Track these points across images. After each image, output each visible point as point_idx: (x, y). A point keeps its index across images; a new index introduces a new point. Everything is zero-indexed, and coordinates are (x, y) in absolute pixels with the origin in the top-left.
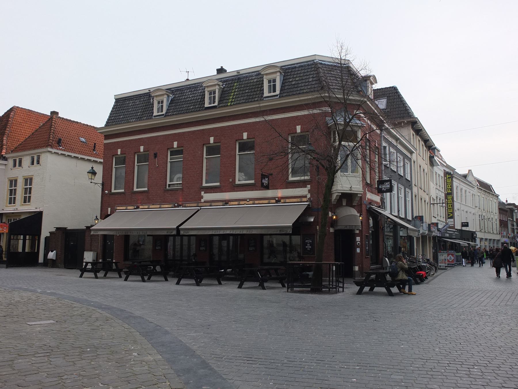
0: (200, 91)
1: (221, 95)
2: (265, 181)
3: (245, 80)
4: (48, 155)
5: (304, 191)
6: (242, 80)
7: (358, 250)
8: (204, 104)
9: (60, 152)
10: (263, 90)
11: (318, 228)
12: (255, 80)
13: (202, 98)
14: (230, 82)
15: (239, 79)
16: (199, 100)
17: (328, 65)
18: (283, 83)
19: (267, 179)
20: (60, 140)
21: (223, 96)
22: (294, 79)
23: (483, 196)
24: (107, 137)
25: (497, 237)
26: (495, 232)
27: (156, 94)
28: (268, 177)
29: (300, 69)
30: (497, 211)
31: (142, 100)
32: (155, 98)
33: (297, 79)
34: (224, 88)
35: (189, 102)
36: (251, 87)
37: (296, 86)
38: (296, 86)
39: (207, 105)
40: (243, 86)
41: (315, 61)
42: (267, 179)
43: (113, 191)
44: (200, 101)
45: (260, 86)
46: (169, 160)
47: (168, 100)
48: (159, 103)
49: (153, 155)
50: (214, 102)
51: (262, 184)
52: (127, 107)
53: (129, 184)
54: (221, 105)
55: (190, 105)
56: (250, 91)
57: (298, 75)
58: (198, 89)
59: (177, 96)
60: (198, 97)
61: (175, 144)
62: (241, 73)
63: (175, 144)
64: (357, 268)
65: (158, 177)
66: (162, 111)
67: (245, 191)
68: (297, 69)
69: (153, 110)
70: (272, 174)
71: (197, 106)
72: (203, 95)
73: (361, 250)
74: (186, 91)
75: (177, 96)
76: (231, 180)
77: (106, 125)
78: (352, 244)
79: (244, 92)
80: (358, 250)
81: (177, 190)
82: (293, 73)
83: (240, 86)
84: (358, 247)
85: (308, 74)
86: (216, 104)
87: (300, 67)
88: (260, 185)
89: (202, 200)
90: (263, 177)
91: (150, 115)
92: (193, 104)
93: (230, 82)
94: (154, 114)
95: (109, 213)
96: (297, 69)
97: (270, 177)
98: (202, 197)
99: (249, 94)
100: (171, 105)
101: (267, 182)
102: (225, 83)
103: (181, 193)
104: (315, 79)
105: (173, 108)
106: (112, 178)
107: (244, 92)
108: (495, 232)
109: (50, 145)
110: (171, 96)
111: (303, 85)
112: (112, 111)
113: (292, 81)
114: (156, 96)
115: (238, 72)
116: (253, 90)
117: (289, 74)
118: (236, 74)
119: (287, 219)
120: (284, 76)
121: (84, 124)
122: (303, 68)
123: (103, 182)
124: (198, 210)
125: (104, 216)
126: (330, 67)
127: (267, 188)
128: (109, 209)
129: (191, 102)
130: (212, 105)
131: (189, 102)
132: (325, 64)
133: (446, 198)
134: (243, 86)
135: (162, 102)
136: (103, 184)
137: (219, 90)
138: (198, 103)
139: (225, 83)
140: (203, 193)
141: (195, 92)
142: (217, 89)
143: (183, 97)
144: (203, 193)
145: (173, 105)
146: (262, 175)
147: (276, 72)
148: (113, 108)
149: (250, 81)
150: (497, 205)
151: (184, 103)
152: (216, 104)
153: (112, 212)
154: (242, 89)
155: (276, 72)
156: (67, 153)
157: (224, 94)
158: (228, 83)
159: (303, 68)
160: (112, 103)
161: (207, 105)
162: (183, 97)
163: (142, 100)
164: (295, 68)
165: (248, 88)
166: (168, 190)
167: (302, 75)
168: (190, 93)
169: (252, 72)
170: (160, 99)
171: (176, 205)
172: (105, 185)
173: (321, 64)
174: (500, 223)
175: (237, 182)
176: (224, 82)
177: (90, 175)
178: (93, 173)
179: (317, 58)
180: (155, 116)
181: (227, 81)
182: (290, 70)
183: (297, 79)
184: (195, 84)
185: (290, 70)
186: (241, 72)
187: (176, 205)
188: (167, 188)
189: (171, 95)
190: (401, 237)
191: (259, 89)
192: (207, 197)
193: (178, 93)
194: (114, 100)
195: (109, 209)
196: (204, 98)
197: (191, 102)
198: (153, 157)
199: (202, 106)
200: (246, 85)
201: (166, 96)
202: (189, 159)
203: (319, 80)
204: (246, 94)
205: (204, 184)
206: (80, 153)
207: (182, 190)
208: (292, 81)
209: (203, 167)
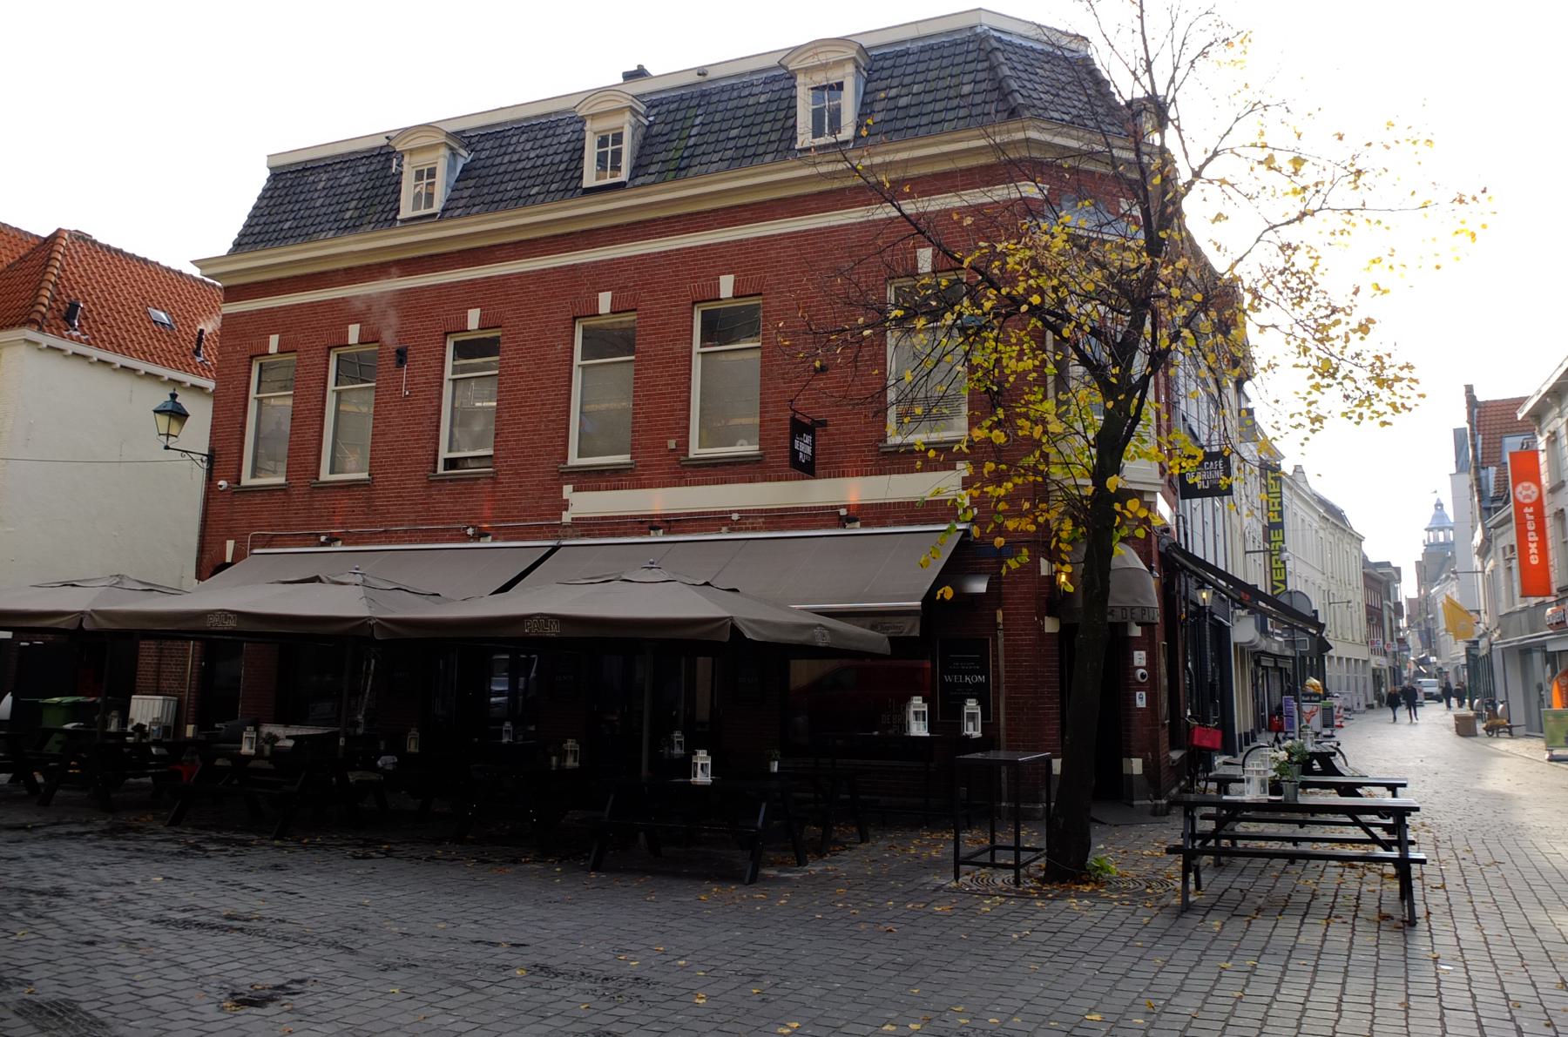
0: (565, 139)
1: (642, 147)
2: (804, 447)
3: (725, 96)
4: (23, 350)
5: (946, 484)
6: (714, 99)
7: (1141, 701)
8: (581, 177)
9: (71, 347)
10: (794, 126)
11: (1000, 619)
12: (763, 99)
13: (571, 160)
14: (674, 106)
15: (703, 95)
16: (562, 167)
17: (1021, 47)
18: (863, 104)
19: (808, 439)
20: (74, 307)
21: (647, 150)
22: (904, 91)
23: (1331, 538)
24: (233, 293)
25: (1362, 653)
26: (1358, 640)
27: (412, 145)
28: (810, 430)
29: (925, 56)
30: (1361, 584)
31: (362, 170)
32: (406, 159)
33: (915, 89)
34: (652, 124)
35: (526, 174)
36: (748, 121)
37: (913, 111)
38: (913, 111)
39: (589, 181)
40: (718, 117)
41: (979, 30)
42: (808, 439)
43: (247, 480)
44: (566, 170)
45: (785, 104)
46: (448, 374)
47: (451, 168)
48: (419, 175)
49: (397, 369)
50: (616, 168)
51: (795, 453)
52: (313, 195)
53: (303, 452)
54: (639, 181)
55: (530, 182)
56: (745, 132)
57: (920, 78)
58: (559, 131)
59: (483, 155)
60: (557, 159)
61: (473, 318)
62: (711, 75)
63: (473, 318)
64: (1136, 766)
65: (406, 425)
66: (430, 204)
67: (725, 482)
68: (912, 59)
69: (398, 200)
70: (823, 424)
71: (554, 187)
72: (575, 150)
73: (1151, 700)
74: (514, 140)
75: (483, 155)
76: (672, 444)
77: (232, 252)
78: (1118, 677)
79: (722, 136)
80: (1141, 701)
81: (475, 479)
82: (897, 72)
83: (709, 118)
84: (1140, 687)
85: (956, 70)
86: (624, 176)
87: (922, 50)
88: (786, 462)
89: (567, 517)
90: (799, 428)
91: (389, 217)
92: (540, 180)
93: (674, 106)
94: (403, 215)
95: (228, 560)
96: (912, 59)
97: (819, 431)
98: (565, 506)
99: (741, 143)
100: (461, 185)
101: (809, 450)
102: (655, 111)
103: (488, 488)
104: (984, 86)
105: (466, 193)
106: (243, 434)
107: (722, 136)
108: (1358, 640)
109: (34, 322)
110: (465, 157)
111: (939, 106)
112: (255, 208)
113: (898, 96)
114: (411, 151)
115: (702, 72)
116: (755, 130)
117: (885, 74)
118: (695, 78)
119: (901, 577)
120: (868, 82)
121: (168, 270)
122: (936, 54)
123: (212, 450)
124: (554, 549)
125: (209, 565)
126: (1032, 55)
127: (808, 470)
128: (230, 544)
129: (535, 172)
130: (609, 181)
131: (526, 174)
132: (1010, 44)
133: (1267, 538)
134: (718, 117)
135: (432, 173)
136: (211, 458)
137: (635, 129)
138: (558, 177)
139: (655, 111)
140: (567, 490)
141: (548, 141)
142: (626, 124)
143: (506, 159)
144: (567, 490)
145: (471, 183)
146: (794, 421)
147: (840, 63)
148: (261, 198)
149: (743, 102)
150: (1360, 564)
151: (507, 177)
152: (624, 176)
153: (239, 556)
154: (716, 127)
155: (840, 63)
156: (96, 354)
157: (648, 143)
158: (664, 109)
159: (936, 54)
160: (261, 178)
161: (589, 181)
162: (506, 159)
163: (362, 170)
164: (906, 53)
165: (738, 123)
166: (442, 480)
167: (932, 75)
168: (529, 146)
169: (753, 73)
170: (423, 161)
171: (470, 531)
172: (220, 459)
173: (999, 40)
174: (1368, 613)
175: (695, 451)
176: (651, 106)
177: (163, 420)
178: (177, 414)
179: (987, 21)
180: (403, 221)
181: (661, 103)
182: (888, 63)
183: (915, 89)
184: (549, 114)
185: (888, 63)
186: (712, 75)
187: (470, 531)
188: (440, 470)
189: (465, 153)
190: (1241, 648)
191: (779, 125)
192: (584, 504)
193: (488, 145)
194: (267, 173)
195: (230, 544)
196: (581, 158)
197: (535, 172)
198: (392, 363)
199: (572, 186)
200: (729, 115)
201: (444, 151)
202: (523, 369)
203: (1001, 91)
204: (731, 144)
205: (574, 460)
206: (147, 356)
207: (494, 479)
208: (898, 96)
209: (567, 429)
